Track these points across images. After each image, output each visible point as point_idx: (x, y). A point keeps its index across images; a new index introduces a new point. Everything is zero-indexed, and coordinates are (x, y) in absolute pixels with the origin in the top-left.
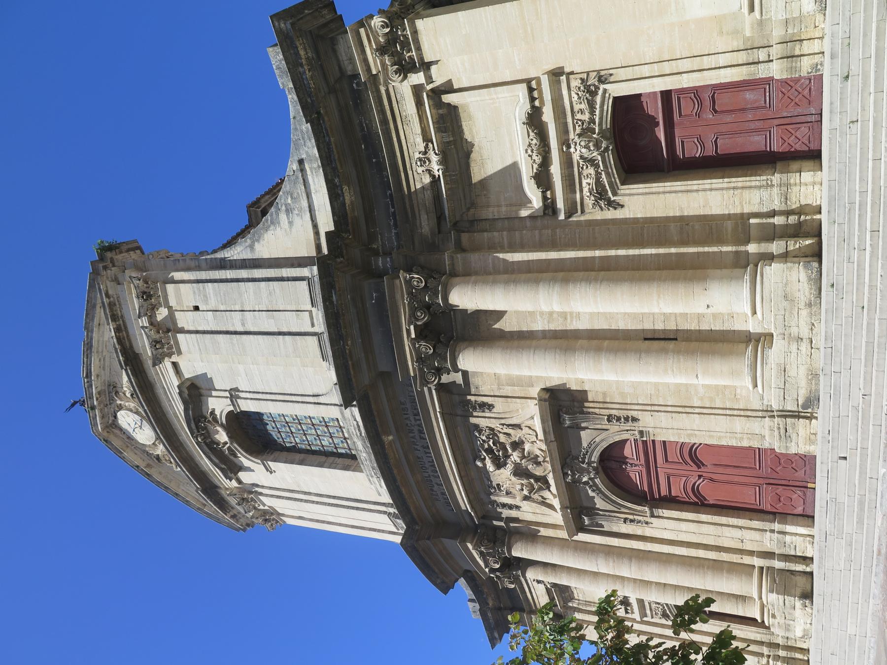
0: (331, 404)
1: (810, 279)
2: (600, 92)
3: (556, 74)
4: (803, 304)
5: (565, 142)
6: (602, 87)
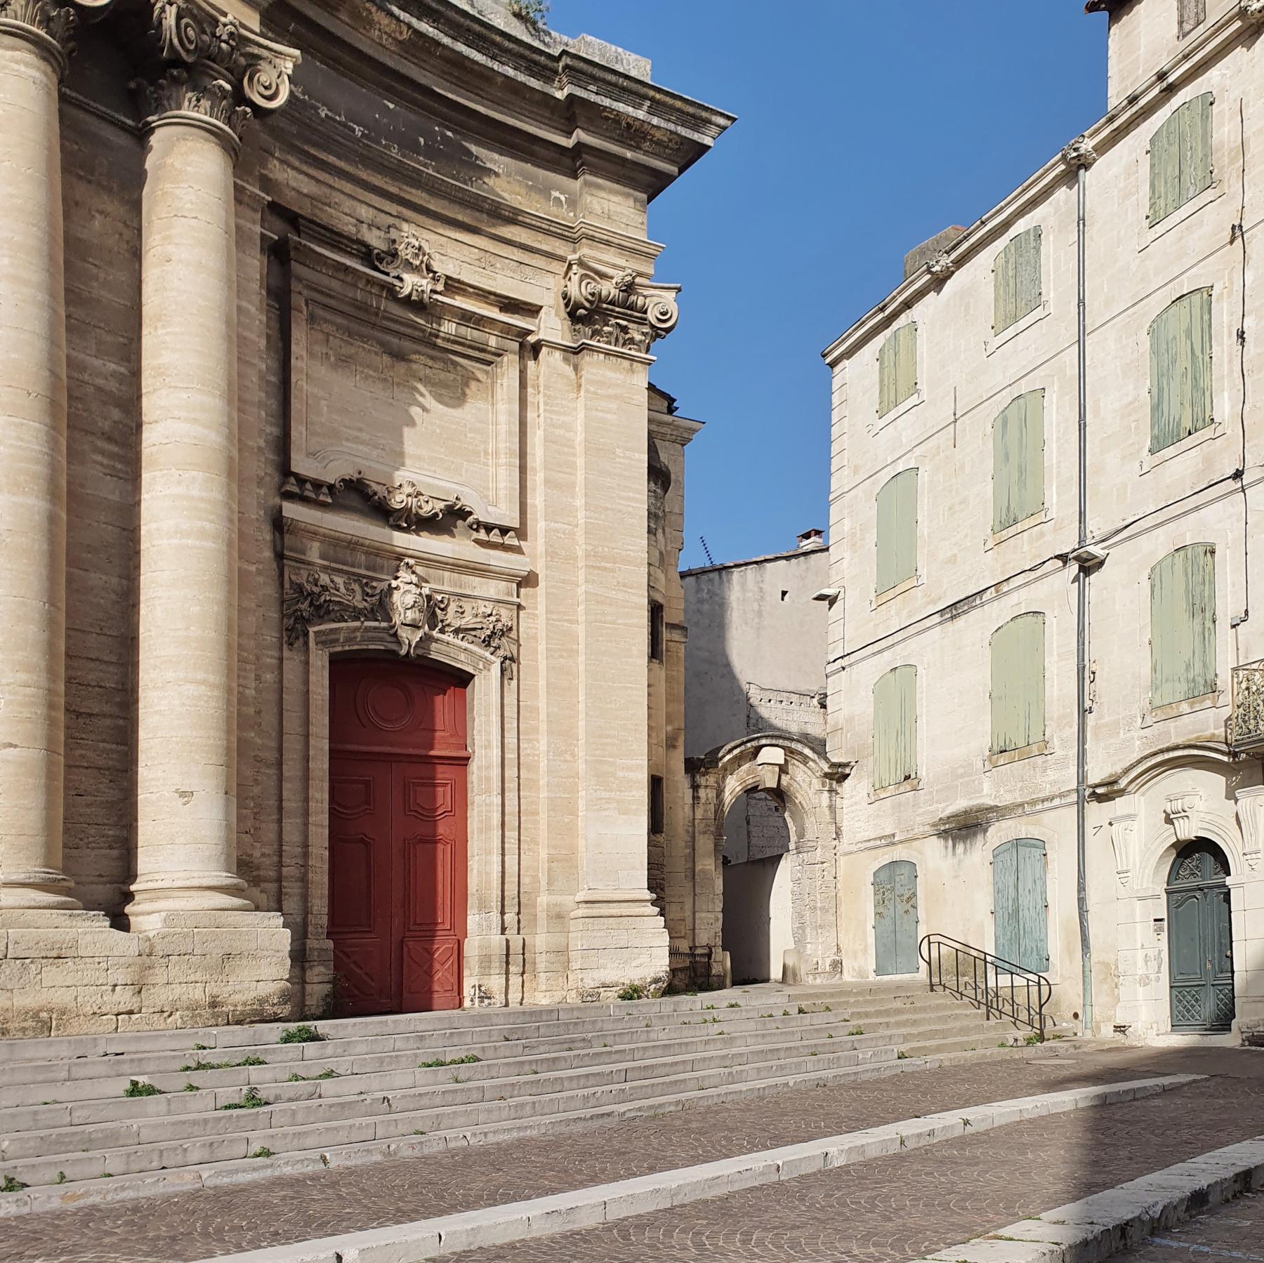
1: (262, 1001)
4: (216, 991)
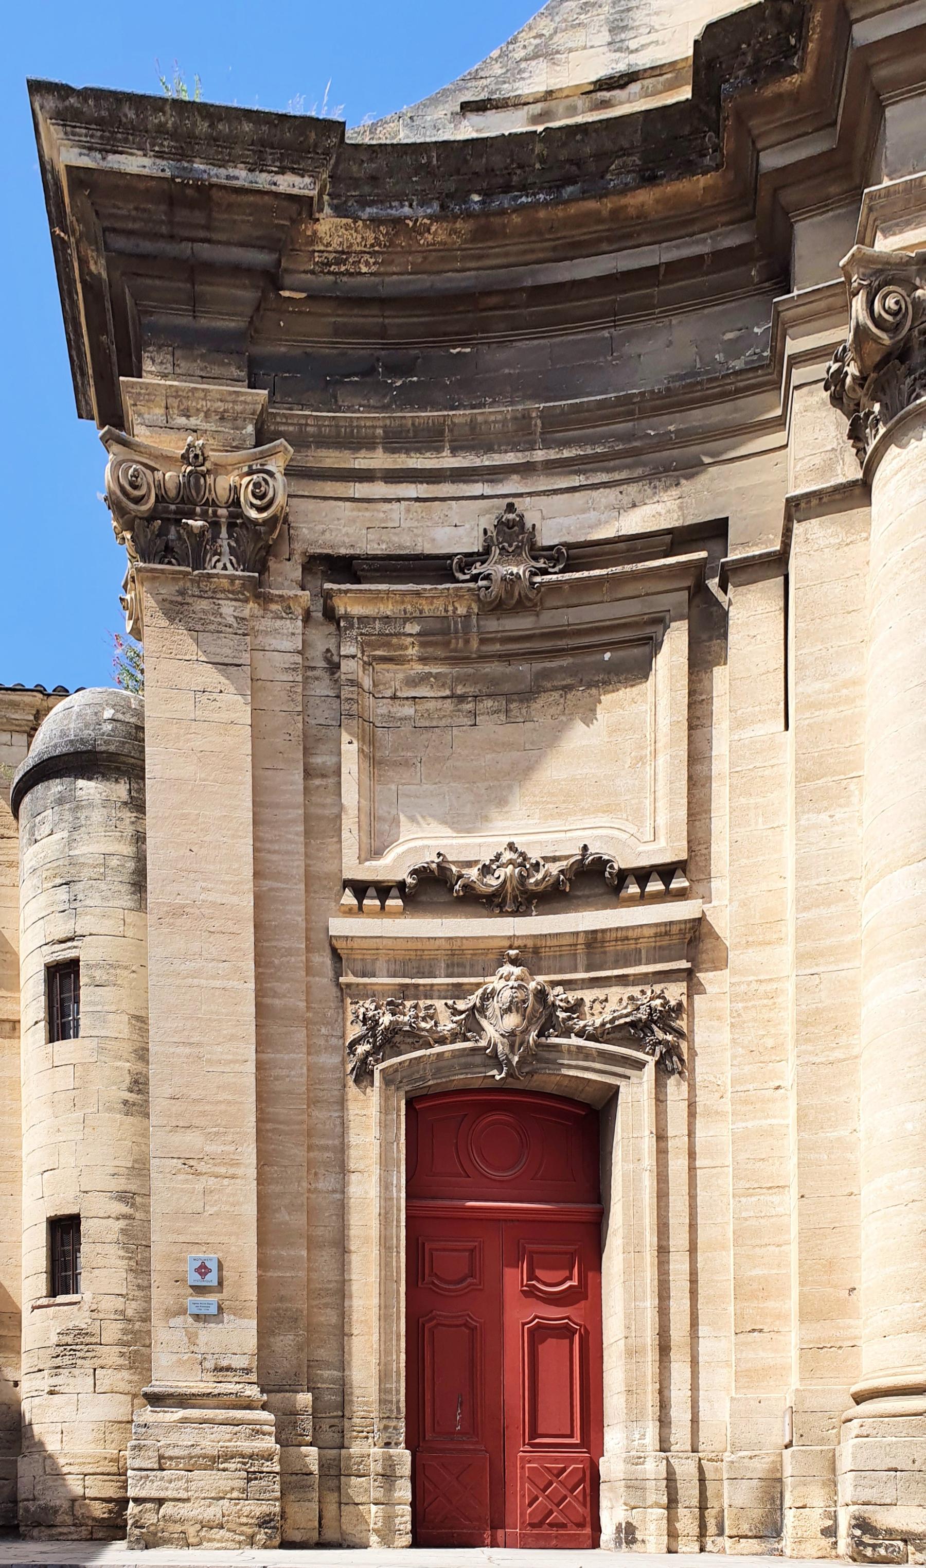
0: (697, 757)
2: (640, 1055)
3: (692, 944)
5: (530, 955)
6: (651, 1061)
